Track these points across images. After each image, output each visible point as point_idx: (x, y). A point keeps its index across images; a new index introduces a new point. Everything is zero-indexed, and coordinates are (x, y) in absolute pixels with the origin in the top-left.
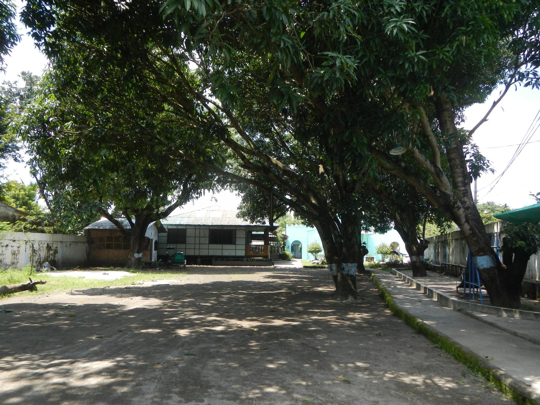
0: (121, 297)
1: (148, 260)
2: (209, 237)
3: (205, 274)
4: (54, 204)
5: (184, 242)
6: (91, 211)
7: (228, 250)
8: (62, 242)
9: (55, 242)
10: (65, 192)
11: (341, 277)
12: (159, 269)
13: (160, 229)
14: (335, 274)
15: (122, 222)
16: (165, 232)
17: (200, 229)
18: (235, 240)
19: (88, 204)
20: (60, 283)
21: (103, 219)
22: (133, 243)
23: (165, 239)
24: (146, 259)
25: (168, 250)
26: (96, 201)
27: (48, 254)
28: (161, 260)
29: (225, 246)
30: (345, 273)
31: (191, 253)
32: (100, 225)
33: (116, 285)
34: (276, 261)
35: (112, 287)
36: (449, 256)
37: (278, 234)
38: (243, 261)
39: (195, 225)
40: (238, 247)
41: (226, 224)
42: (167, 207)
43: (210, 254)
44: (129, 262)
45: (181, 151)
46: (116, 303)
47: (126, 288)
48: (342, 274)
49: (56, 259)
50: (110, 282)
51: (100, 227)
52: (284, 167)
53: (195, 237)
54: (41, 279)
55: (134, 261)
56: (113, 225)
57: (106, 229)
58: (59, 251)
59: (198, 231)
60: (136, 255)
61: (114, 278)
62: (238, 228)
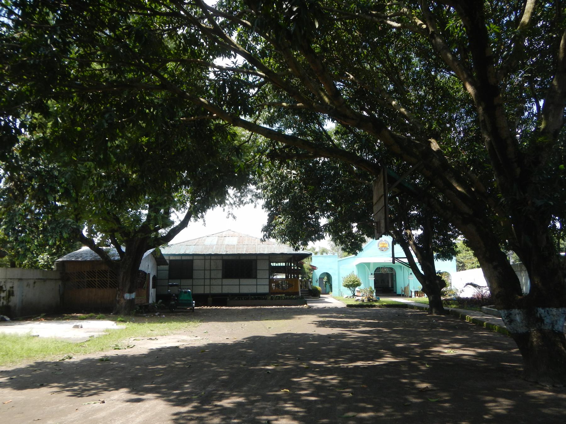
5: (190, 276)
8: (20, 279)
9: (9, 280)
10: (23, 207)
12: (159, 315)
13: (159, 259)
15: (108, 251)
16: (166, 264)
17: (211, 259)
18: (256, 273)
19: (57, 224)
22: (123, 279)
25: (170, 288)
26: (68, 220)
28: (160, 301)
29: (244, 281)
30: (547, 328)
31: (200, 290)
37: (304, 265)
38: (266, 299)
39: (204, 255)
40: (260, 282)
43: (224, 292)
44: (118, 305)
47: (101, 360)
48: (540, 330)
49: (10, 304)
50: (77, 345)
51: (78, 258)
54: (263, 245)
55: (124, 305)
56: (97, 255)
57: (86, 262)
58: (15, 293)
60: (127, 296)
62: (259, 257)
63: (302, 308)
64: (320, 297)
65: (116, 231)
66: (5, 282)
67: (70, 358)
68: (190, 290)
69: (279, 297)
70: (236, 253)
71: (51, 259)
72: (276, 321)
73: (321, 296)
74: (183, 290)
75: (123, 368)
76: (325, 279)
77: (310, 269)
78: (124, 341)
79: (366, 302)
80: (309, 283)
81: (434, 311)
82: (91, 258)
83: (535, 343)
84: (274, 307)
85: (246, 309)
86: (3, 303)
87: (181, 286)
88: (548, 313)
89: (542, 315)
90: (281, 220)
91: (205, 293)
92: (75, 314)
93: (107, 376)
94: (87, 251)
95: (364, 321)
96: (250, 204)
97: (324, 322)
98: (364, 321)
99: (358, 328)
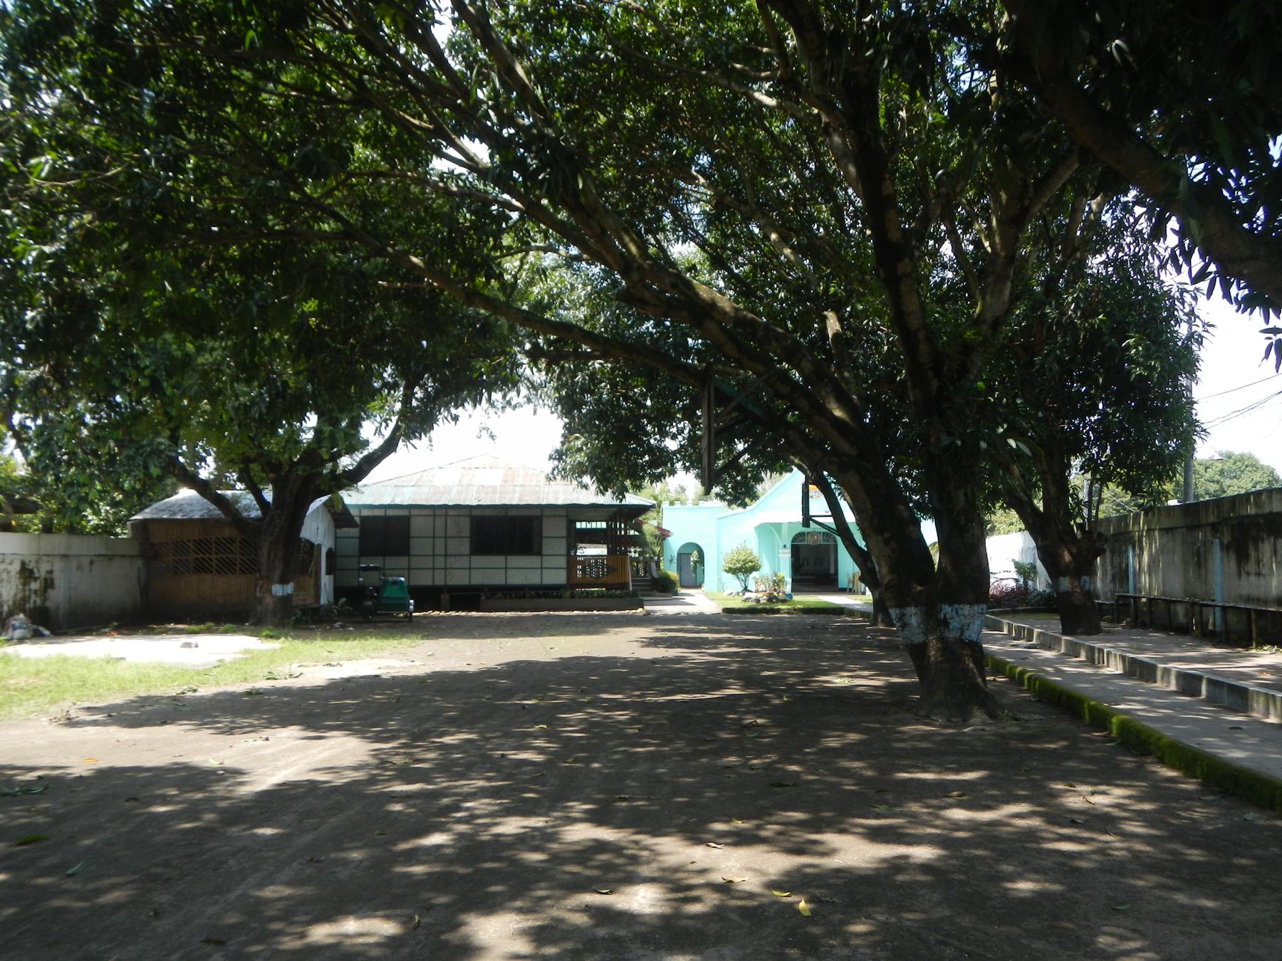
0: (230, 731)
1: (310, 601)
2: (471, 537)
3: (474, 638)
4: (37, 449)
5: (404, 551)
6: (146, 468)
7: (522, 571)
8: (65, 556)
9: (45, 558)
10: (69, 415)
11: (938, 650)
12: (342, 626)
13: (340, 516)
14: (918, 639)
15: (236, 499)
17: (446, 516)
19: (138, 449)
20: (42, 682)
21: (186, 493)
22: (269, 558)
23: (352, 545)
24: (305, 599)
25: (362, 573)
26: (160, 440)
27: (24, 590)
28: (343, 600)
29: (515, 561)
30: (952, 635)
31: (423, 579)
32: (176, 509)
33: (218, 684)
34: (649, 595)
35: (206, 691)
36: (1137, 575)
37: (645, 527)
38: (561, 597)
40: (548, 562)
41: (515, 502)
42: (359, 456)
43: (473, 582)
44: (259, 608)
45: (414, 259)
46: (210, 761)
47: (249, 693)
48: (942, 639)
49: (48, 604)
50: (198, 673)
51: (175, 514)
52: (737, 310)
53: (434, 537)
56: (213, 507)
57: (191, 521)
58: (57, 582)
59: (440, 523)
60: (278, 590)
61: (213, 660)
62: (546, 512)
63: (633, 616)
64: (676, 594)
65: (254, 461)
66: (37, 562)
67: (195, 691)
68: (403, 579)
69: (587, 592)
70: (498, 502)
71: (114, 514)
72: (568, 638)
74: (390, 579)
75: (287, 704)
76: (694, 557)
78: (280, 669)
80: (653, 565)
81: (880, 618)
82: (201, 513)
83: (933, 659)
84: (576, 613)
85: (519, 617)
86: (35, 602)
87: (384, 569)
88: (957, 613)
89: (948, 616)
90: (579, 443)
91: (436, 583)
92: (172, 625)
93: (264, 713)
94: (191, 499)
95: (737, 637)
96: (526, 406)
97: (661, 638)
98: (737, 637)
99: (717, 648)
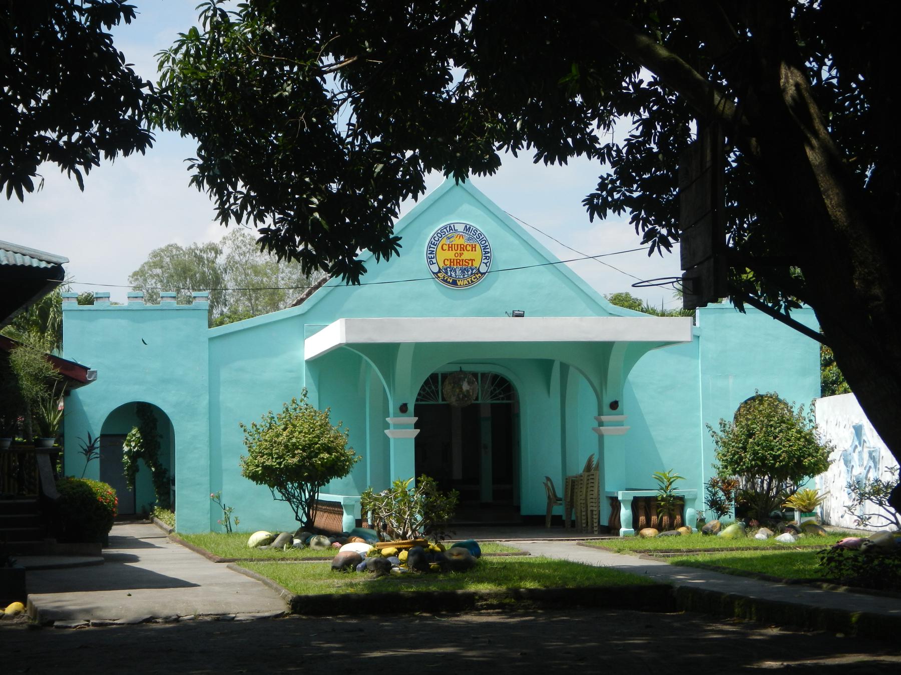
37: (19, 356)
73: (118, 530)
77: (49, 382)
79: (406, 578)
80: (43, 461)
